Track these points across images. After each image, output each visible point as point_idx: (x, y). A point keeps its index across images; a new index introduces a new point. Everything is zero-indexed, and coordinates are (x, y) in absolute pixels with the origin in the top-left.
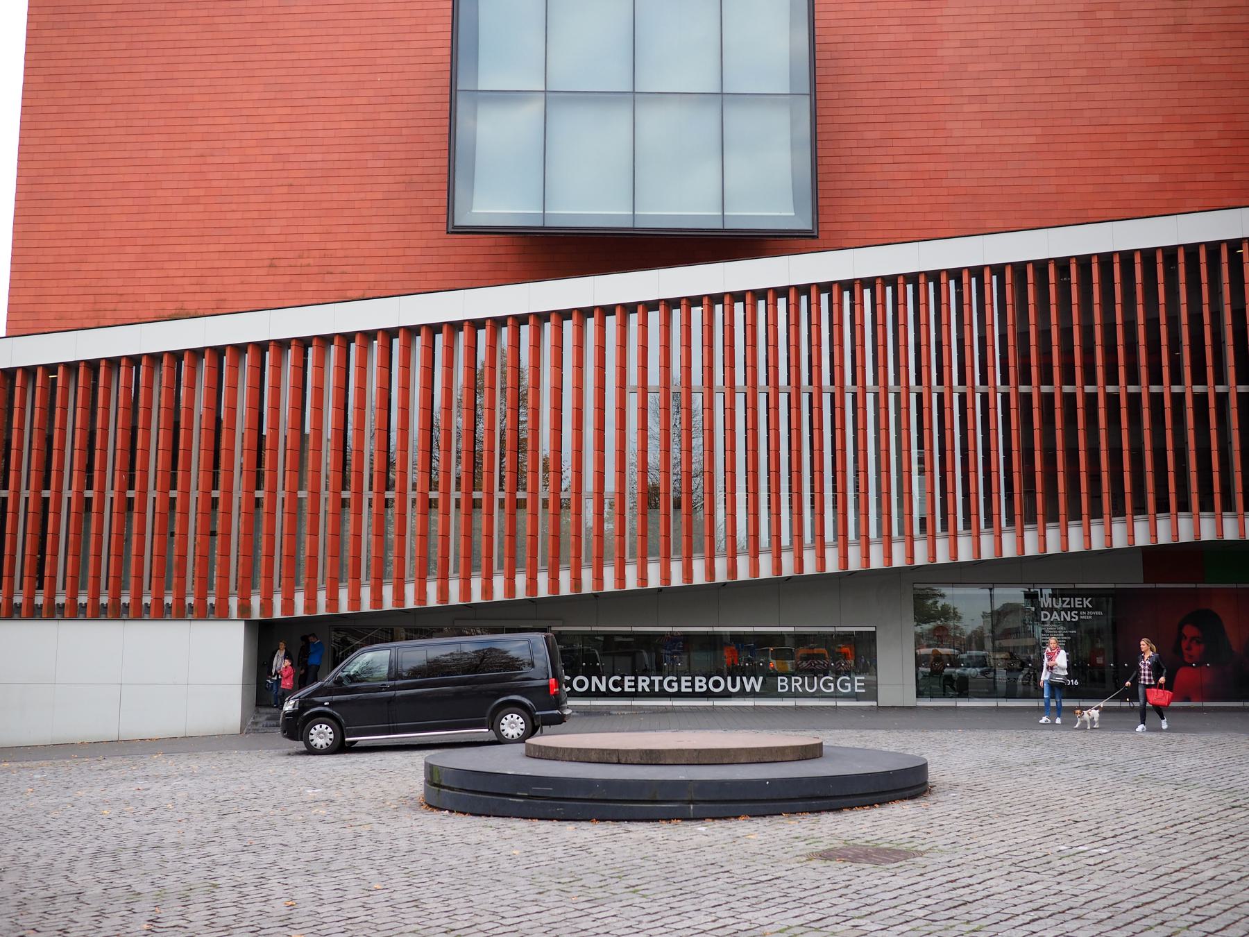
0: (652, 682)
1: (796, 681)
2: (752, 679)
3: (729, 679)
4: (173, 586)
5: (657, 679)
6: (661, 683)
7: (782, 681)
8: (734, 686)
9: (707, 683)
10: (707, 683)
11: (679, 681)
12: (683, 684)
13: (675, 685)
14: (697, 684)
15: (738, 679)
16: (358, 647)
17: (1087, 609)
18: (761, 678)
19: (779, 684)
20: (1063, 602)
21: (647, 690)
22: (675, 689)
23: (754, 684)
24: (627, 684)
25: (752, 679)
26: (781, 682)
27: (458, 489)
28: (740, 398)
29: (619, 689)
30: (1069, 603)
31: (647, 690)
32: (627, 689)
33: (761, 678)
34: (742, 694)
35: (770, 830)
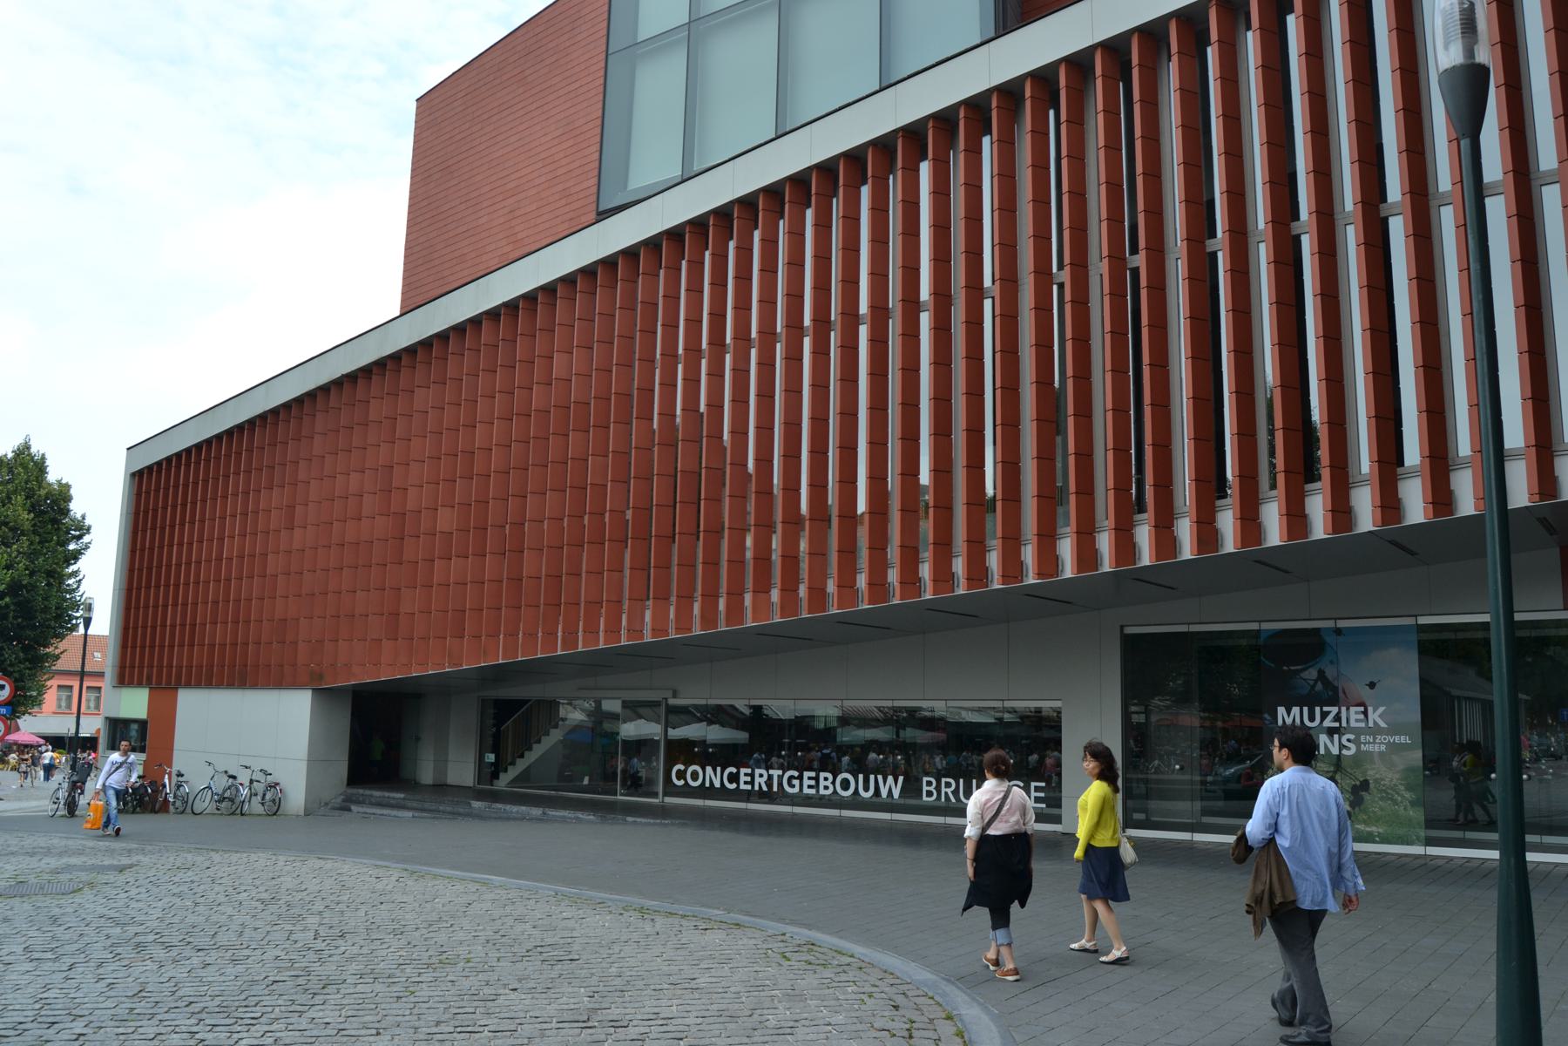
0: (770, 777)
1: (948, 785)
2: (890, 778)
3: (861, 777)
4: (930, 155)
5: (776, 773)
6: (780, 778)
7: (929, 784)
8: (866, 789)
9: (833, 783)
10: (833, 783)
11: (800, 778)
12: (806, 782)
13: (796, 782)
14: (822, 783)
15: (872, 777)
16: (714, 745)
17: (1375, 731)
18: (901, 779)
19: (925, 788)
20: (1324, 715)
21: (765, 788)
22: (796, 790)
23: (891, 787)
24: (743, 778)
25: (890, 778)
26: (927, 783)
27: (1135, 272)
28: (925, 320)
29: (734, 786)
30: (1338, 718)
31: (765, 788)
32: (743, 787)
33: (901, 779)
34: (875, 804)
35: (391, 878)
